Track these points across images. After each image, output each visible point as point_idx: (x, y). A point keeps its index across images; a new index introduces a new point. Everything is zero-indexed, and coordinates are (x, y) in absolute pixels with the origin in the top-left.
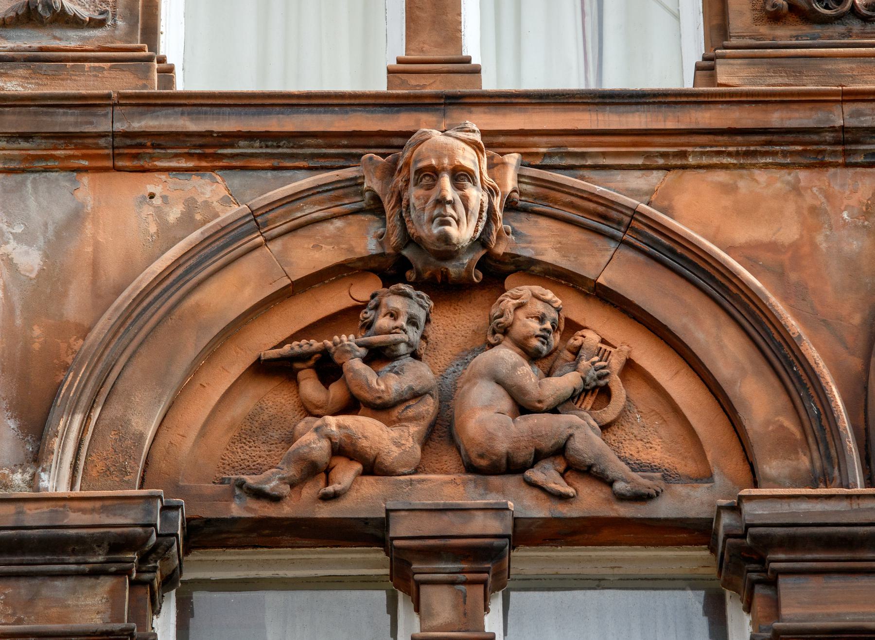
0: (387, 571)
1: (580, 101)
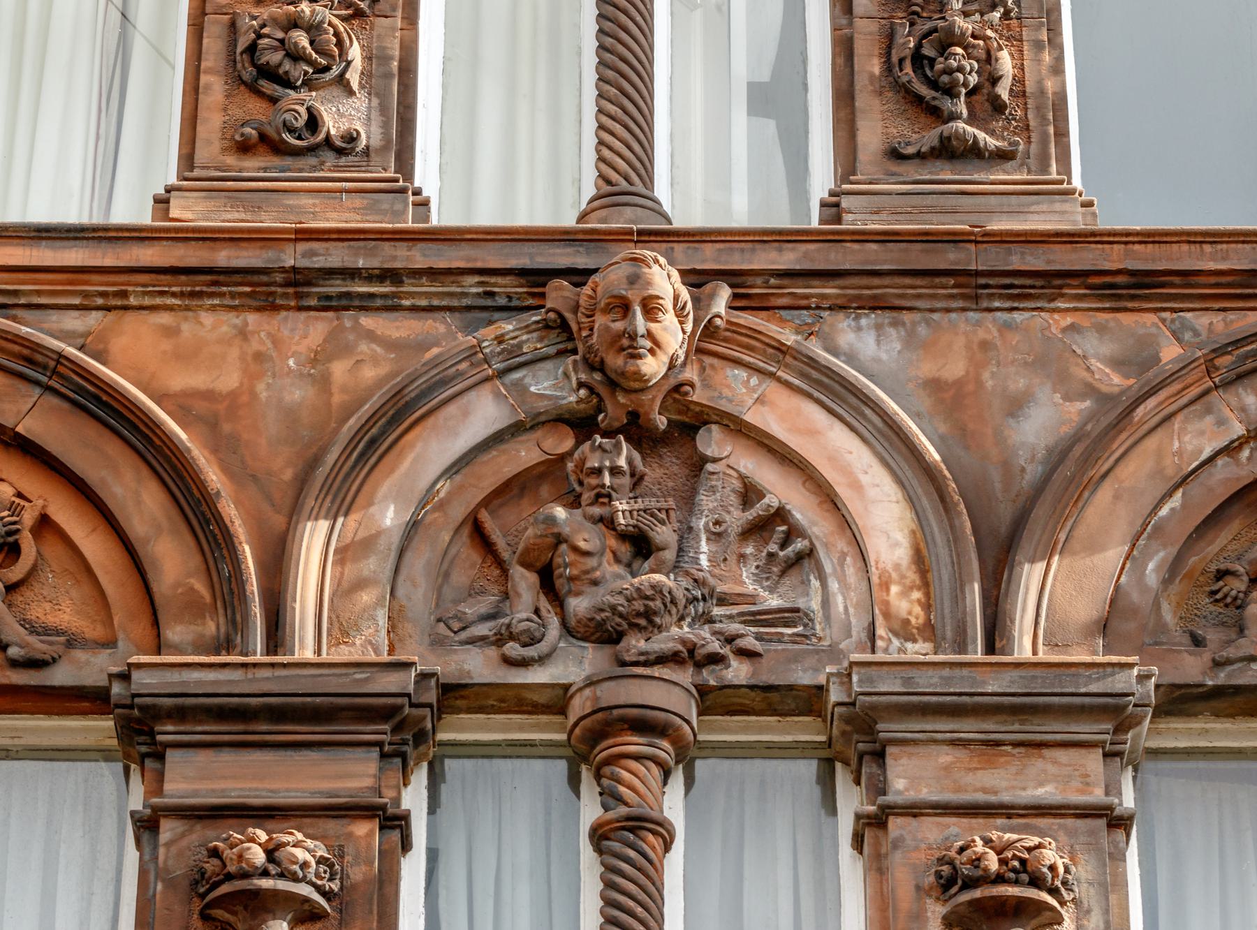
1: (14, 234)
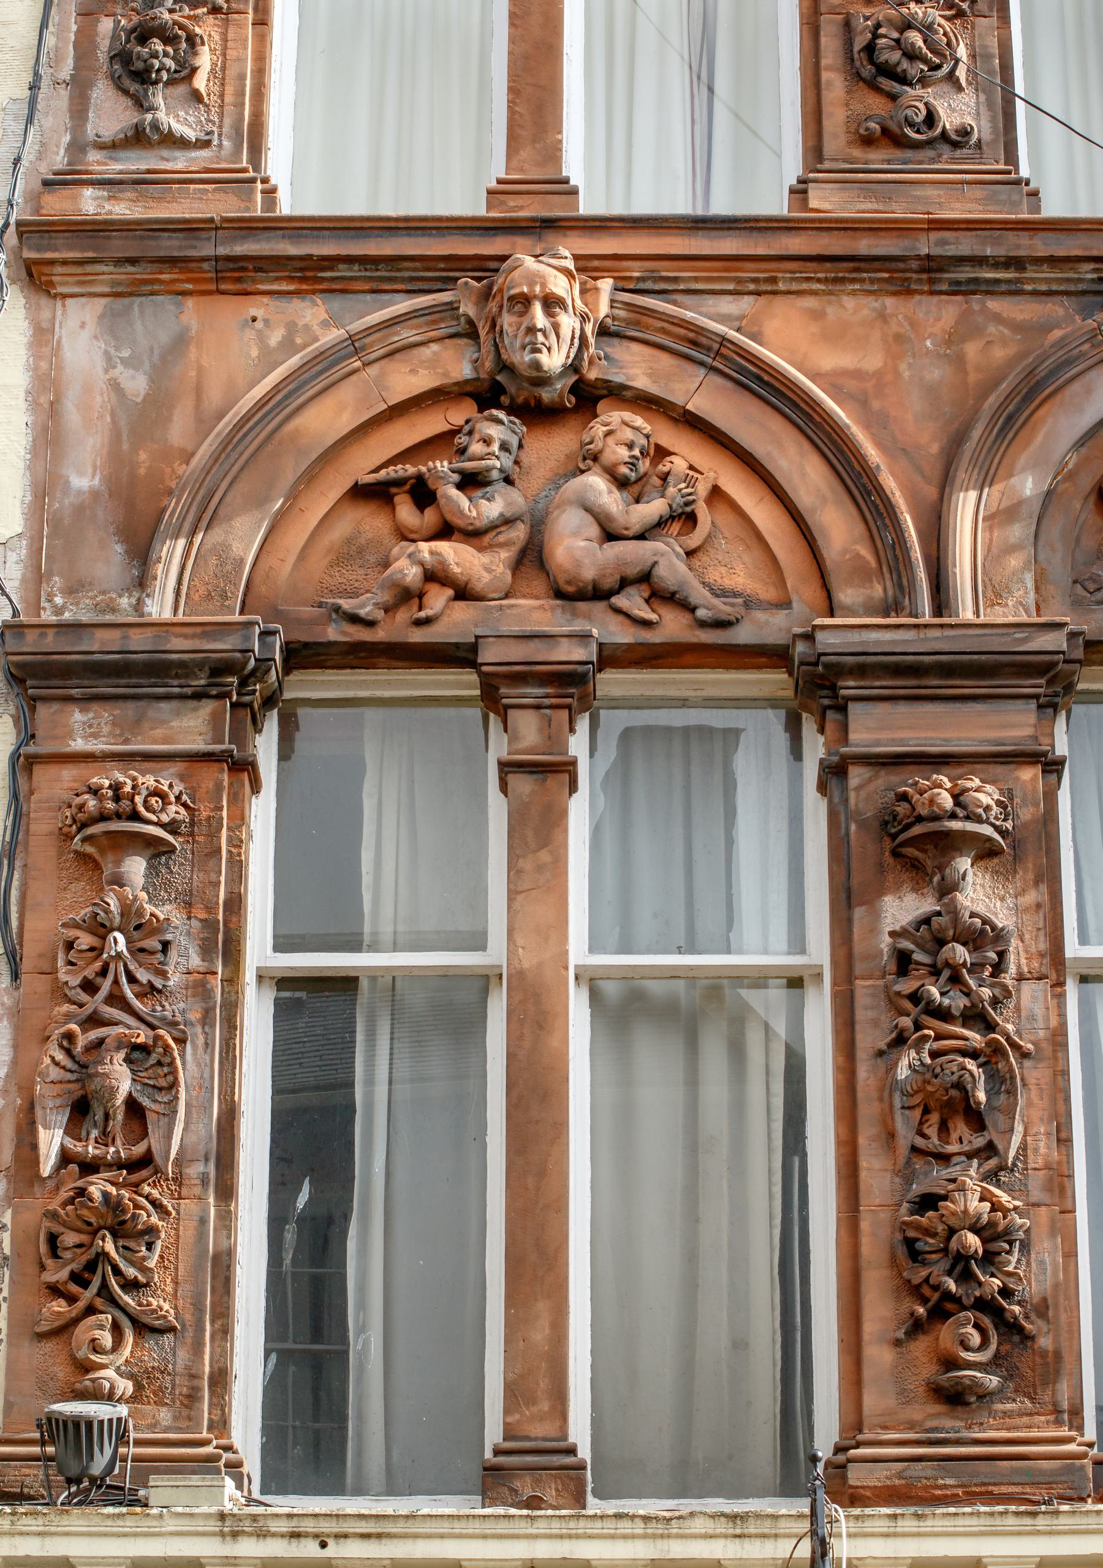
0: (478, 692)
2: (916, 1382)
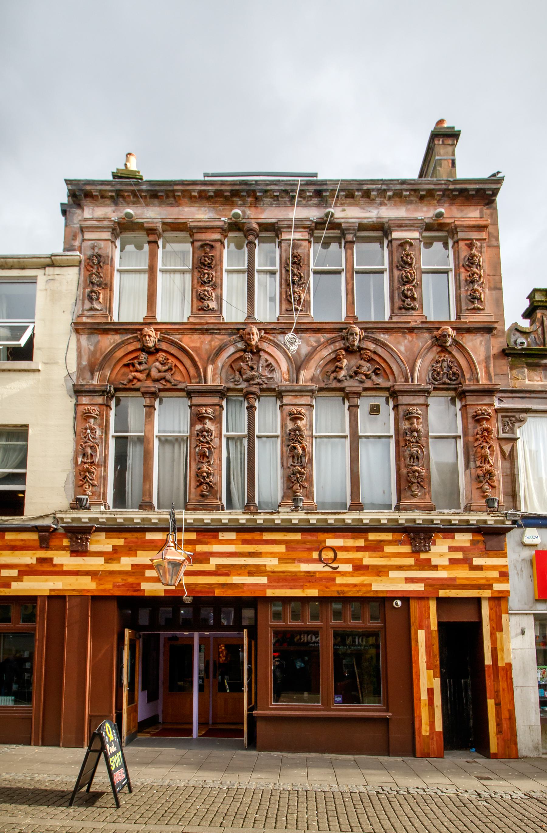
2: (198, 495)
